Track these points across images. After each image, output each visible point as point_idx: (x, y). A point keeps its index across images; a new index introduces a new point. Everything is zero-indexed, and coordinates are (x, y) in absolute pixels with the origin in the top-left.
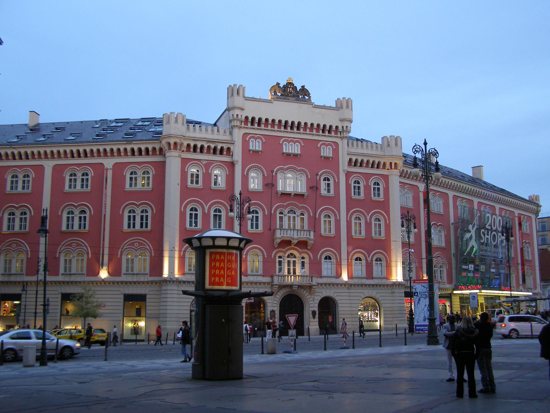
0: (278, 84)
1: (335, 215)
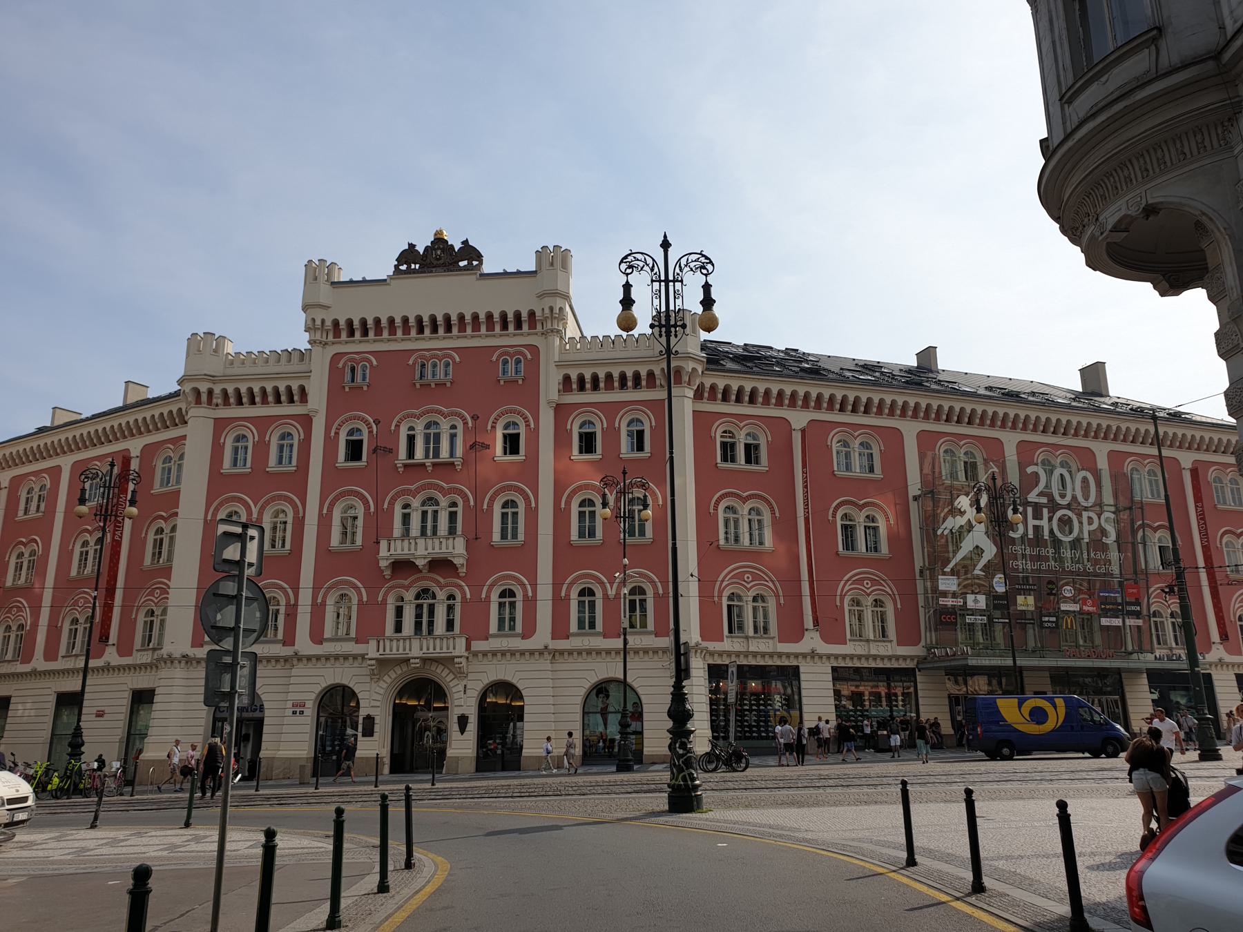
0: (412, 246)
1: (527, 498)
